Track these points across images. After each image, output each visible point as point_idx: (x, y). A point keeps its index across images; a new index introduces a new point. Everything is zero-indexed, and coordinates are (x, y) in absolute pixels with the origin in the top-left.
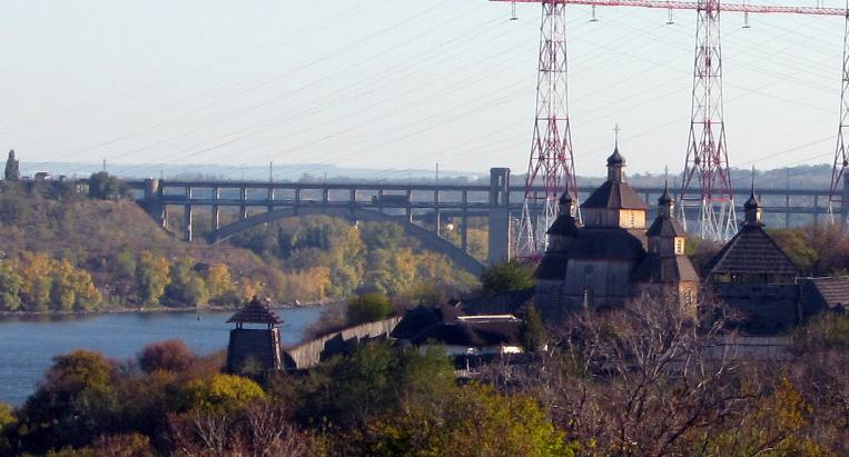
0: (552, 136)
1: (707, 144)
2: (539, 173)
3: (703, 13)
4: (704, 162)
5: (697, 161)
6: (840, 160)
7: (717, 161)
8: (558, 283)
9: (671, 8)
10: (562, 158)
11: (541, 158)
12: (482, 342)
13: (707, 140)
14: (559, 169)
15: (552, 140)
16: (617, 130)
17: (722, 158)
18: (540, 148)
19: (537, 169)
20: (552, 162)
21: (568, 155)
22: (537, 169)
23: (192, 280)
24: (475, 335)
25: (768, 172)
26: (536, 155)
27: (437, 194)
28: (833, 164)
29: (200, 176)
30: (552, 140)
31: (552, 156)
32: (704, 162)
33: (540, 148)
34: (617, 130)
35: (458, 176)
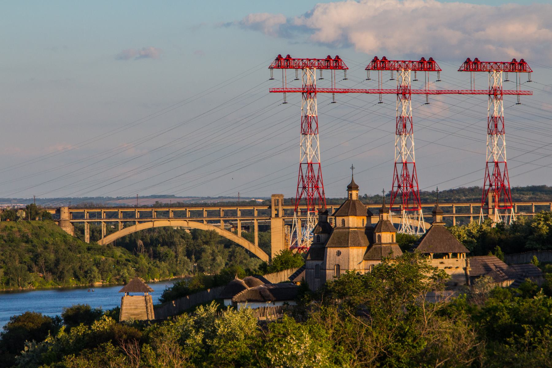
0: (310, 174)
1: (405, 176)
2: (303, 196)
3: (401, 96)
4: (404, 187)
5: (399, 186)
6: (488, 183)
7: (412, 186)
8: (320, 262)
9: (380, 93)
10: (317, 187)
11: (304, 188)
12: (274, 299)
13: (405, 174)
14: (315, 193)
15: (310, 176)
16: (352, 168)
17: (415, 184)
18: (303, 181)
19: (302, 194)
20: (310, 189)
21: (320, 185)
22: (302, 194)
23: (106, 259)
24: (268, 291)
25: (289, 198)
26: (301, 185)
27: (334, 94)
28: (483, 187)
29: (128, 205)
30: (310, 176)
31: (310, 186)
32: (404, 187)
33: (303, 181)
34: (352, 168)
35: (24, 312)
